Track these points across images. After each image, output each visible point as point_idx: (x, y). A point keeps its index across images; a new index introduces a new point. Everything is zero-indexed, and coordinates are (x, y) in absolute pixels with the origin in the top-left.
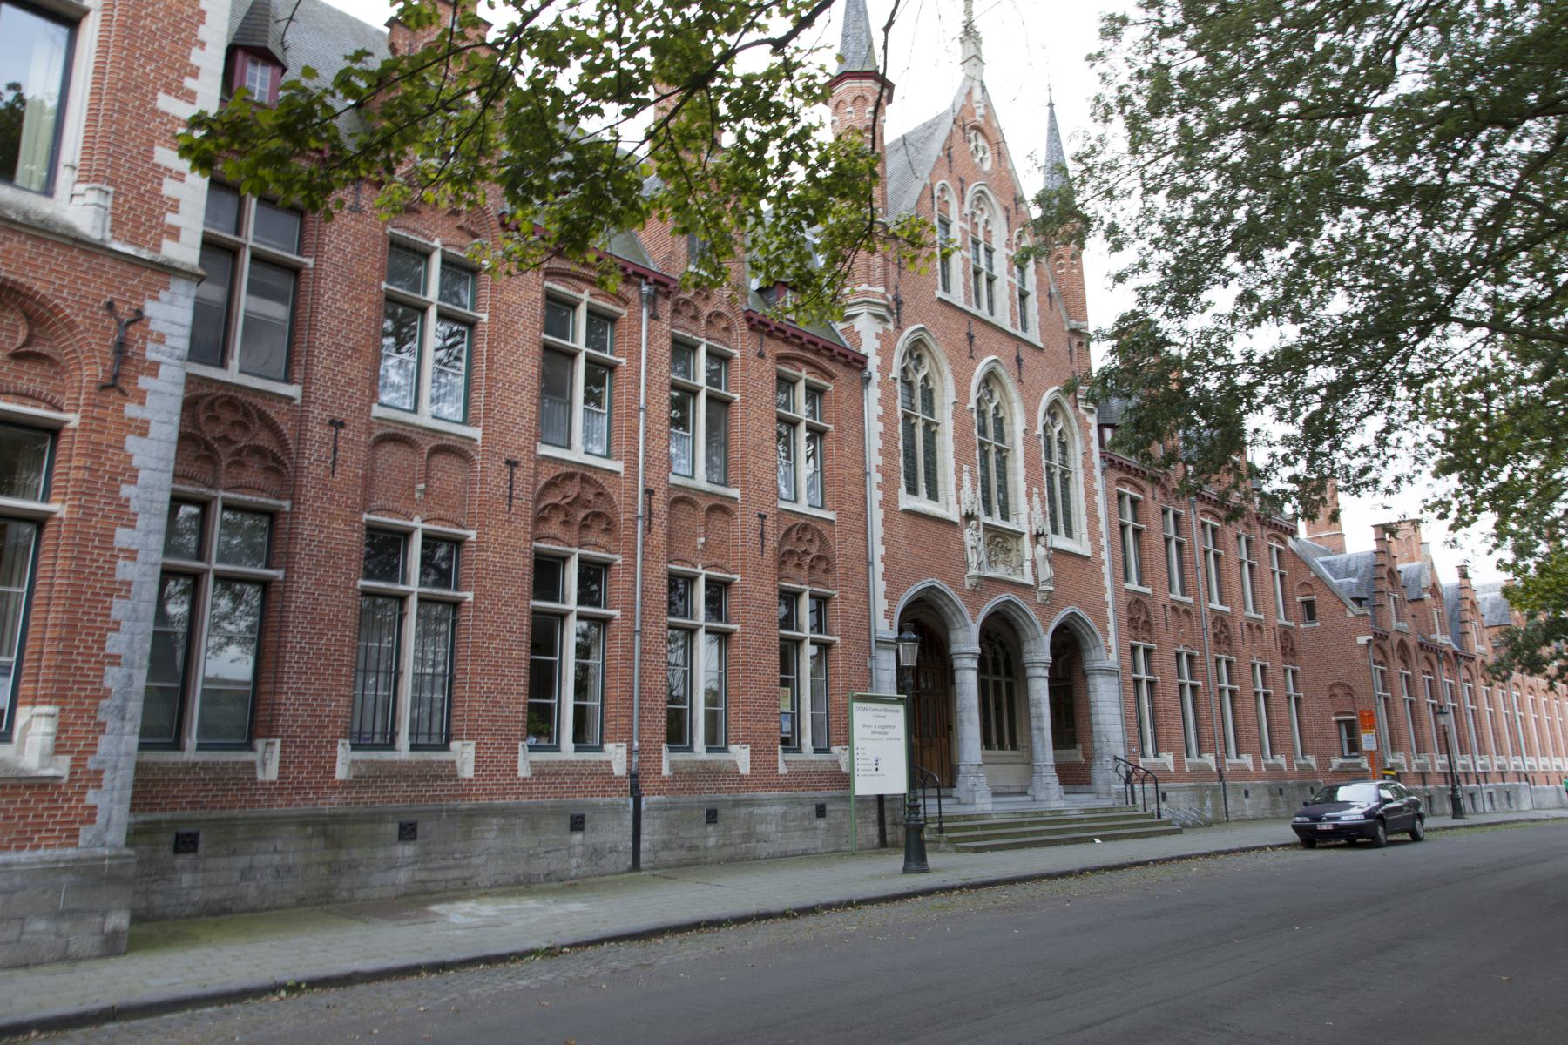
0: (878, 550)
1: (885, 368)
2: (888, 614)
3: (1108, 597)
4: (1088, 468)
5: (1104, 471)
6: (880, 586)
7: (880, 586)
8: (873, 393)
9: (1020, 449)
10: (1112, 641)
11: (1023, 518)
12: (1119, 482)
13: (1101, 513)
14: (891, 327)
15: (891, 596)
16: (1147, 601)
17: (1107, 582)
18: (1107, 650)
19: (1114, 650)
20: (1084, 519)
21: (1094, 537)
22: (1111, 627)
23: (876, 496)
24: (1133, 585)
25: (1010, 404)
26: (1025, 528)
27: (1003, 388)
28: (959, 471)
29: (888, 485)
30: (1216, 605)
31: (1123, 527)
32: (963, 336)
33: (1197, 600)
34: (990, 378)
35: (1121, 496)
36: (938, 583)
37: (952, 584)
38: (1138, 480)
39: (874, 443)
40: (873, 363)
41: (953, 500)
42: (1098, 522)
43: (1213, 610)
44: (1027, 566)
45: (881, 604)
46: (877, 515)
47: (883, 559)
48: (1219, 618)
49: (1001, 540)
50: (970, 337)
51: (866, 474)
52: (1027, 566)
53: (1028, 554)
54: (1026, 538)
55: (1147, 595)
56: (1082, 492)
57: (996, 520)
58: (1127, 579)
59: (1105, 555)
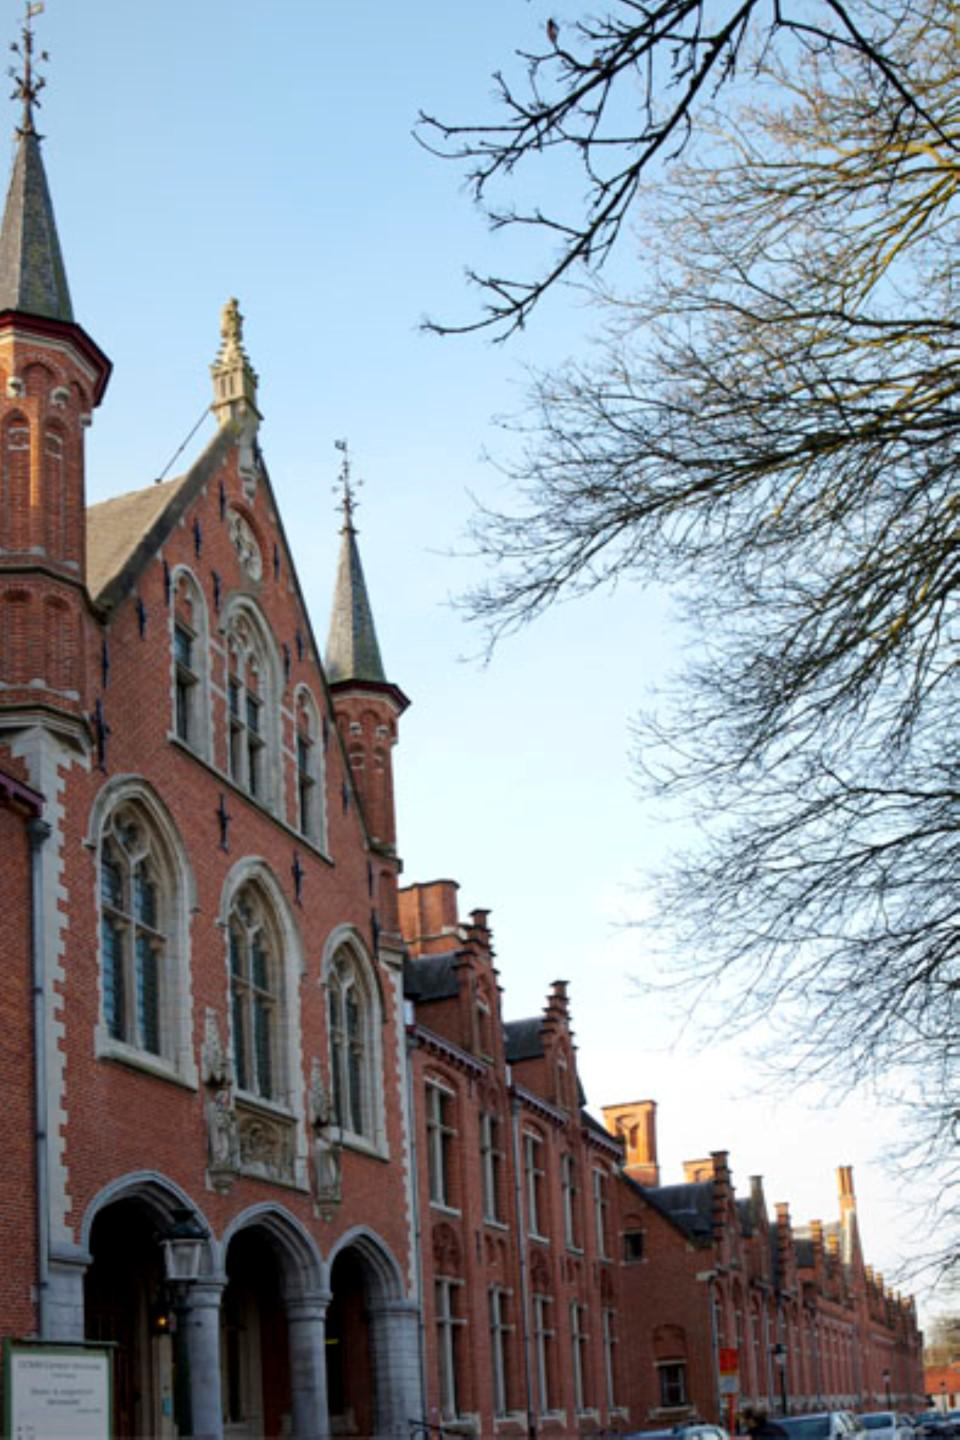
0: (54, 1117)
1: (73, 827)
2: (71, 1219)
3: (410, 1217)
4: (389, 1045)
5: (409, 1049)
6: (55, 1175)
7: (55, 1175)
8: (50, 863)
9: (294, 1002)
10: (412, 1274)
11: (297, 1099)
12: (429, 1069)
13: (404, 1105)
14: (86, 763)
15: (78, 1189)
16: (456, 1228)
17: (409, 1197)
18: (411, 1282)
19: (415, 1285)
20: (382, 1112)
21: (394, 1136)
22: (412, 1256)
23: (51, 1030)
24: (439, 1205)
25: (279, 933)
26: (299, 1112)
27: (270, 908)
28: (198, 1015)
29: (76, 1012)
30: (535, 1236)
31: (430, 1129)
32: (210, 813)
33: (515, 1228)
34: (252, 889)
35: (429, 1088)
36: (162, 1179)
37: (183, 1181)
38: (451, 1071)
39: (51, 945)
40: (52, 812)
41: (188, 1055)
42: (400, 1117)
43: (532, 1242)
44: (300, 1167)
45: (57, 1201)
46: (52, 1064)
47: (64, 1131)
48: (536, 1252)
49: (262, 1128)
50: (223, 819)
51: (35, 991)
52: (300, 1167)
53: (302, 1144)
54: (300, 1127)
55: (454, 1216)
56: (380, 1075)
57: (253, 1096)
58: (432, 1196)
59: (407, 1162)
